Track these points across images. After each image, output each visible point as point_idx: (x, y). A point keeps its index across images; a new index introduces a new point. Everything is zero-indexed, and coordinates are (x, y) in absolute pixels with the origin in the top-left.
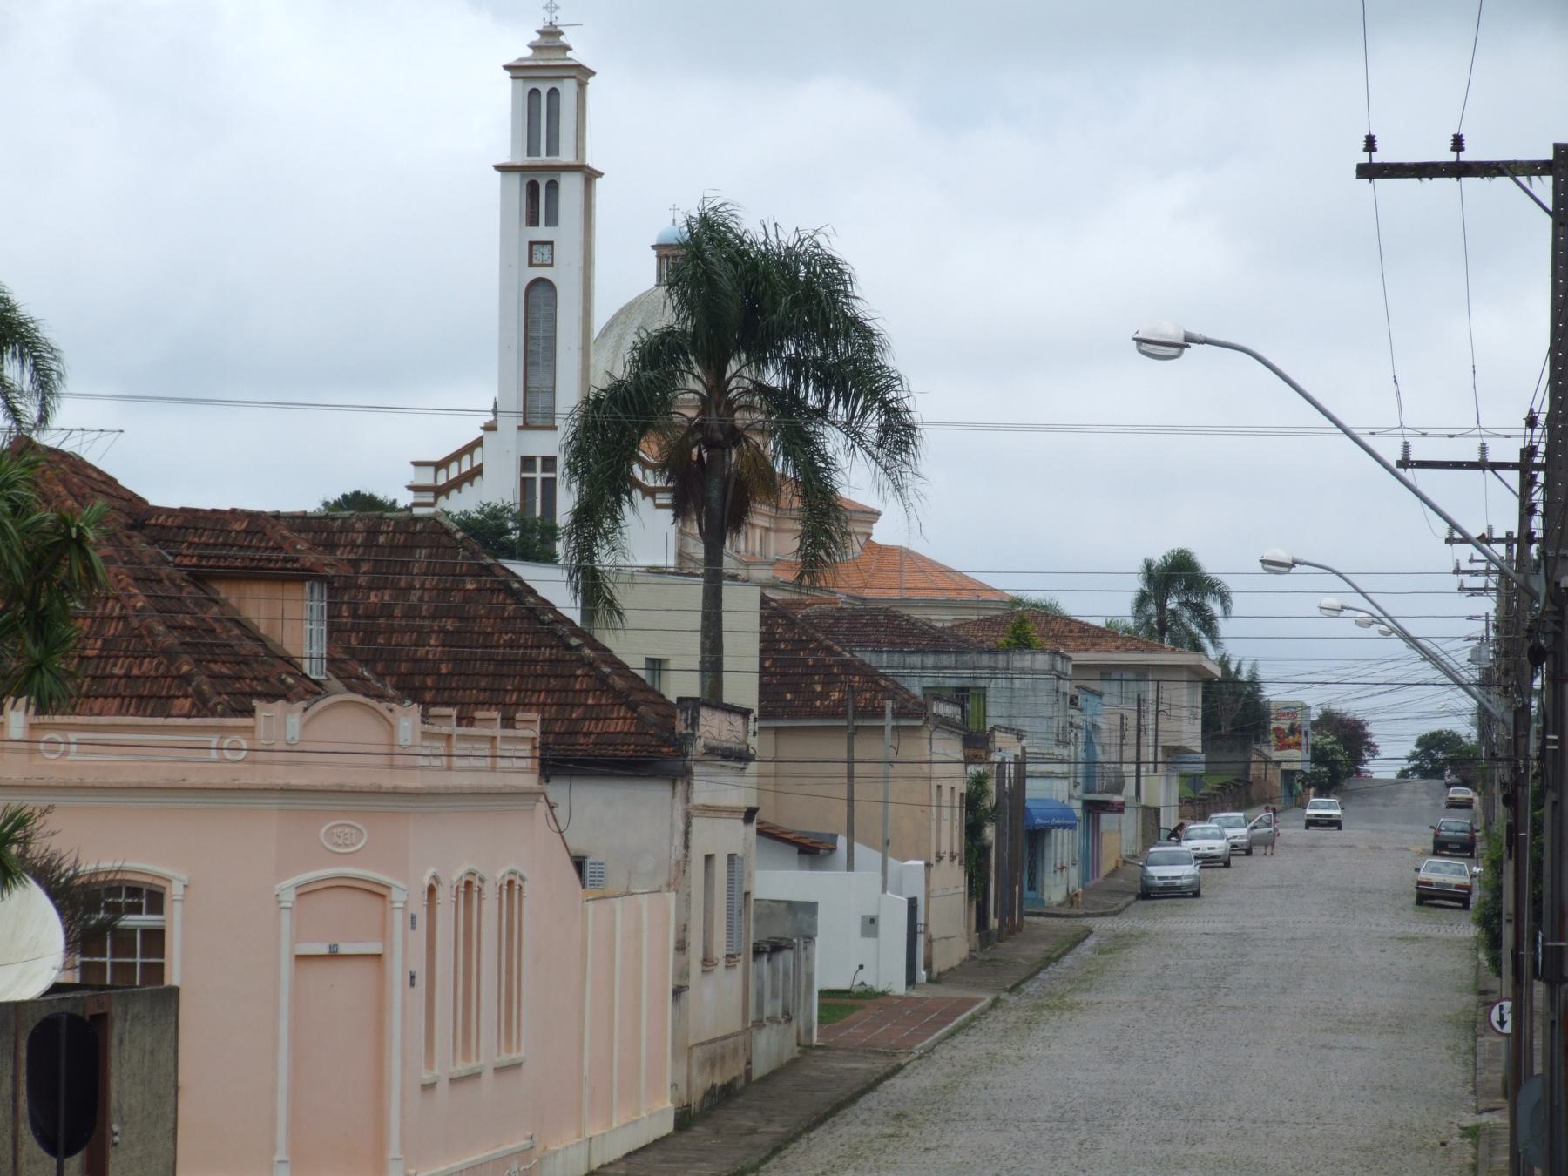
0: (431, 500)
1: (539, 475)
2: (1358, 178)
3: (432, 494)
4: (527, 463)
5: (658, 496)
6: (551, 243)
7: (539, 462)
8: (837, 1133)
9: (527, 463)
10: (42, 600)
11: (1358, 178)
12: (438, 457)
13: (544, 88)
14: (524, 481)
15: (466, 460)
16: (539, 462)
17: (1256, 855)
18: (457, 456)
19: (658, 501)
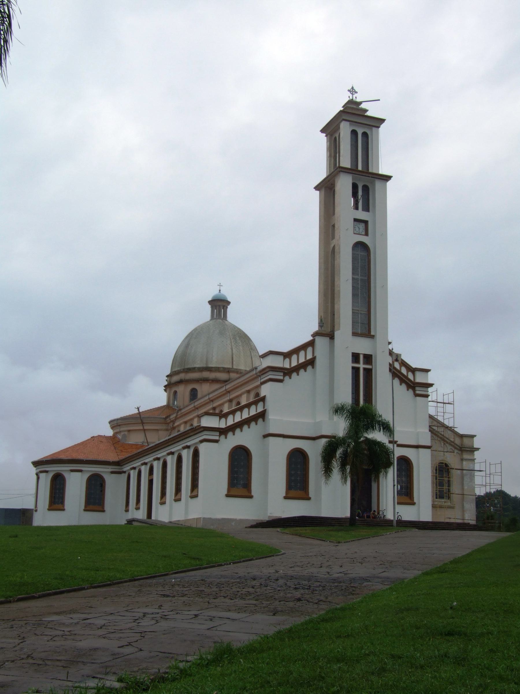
0: (281, 378)
1: (362, 366)
2: (401, 354)
3: (282, 374)
4: (356, 357)
5: (417, 388)
6: (354, 233)
7: (361, 357)
8: (272, 570)
9: (356, 357)
10: (362, 438)
11: (401, 354)
12: (286, 349)
13: (360, 132)
14: (353, 368)
15: (302, 353)
16: (361, 357)
17: (386, 514)
18: (296, 351)
19: (417, 392)
